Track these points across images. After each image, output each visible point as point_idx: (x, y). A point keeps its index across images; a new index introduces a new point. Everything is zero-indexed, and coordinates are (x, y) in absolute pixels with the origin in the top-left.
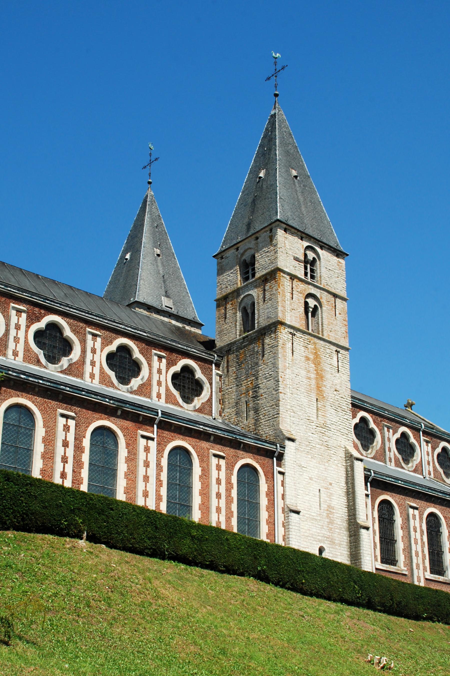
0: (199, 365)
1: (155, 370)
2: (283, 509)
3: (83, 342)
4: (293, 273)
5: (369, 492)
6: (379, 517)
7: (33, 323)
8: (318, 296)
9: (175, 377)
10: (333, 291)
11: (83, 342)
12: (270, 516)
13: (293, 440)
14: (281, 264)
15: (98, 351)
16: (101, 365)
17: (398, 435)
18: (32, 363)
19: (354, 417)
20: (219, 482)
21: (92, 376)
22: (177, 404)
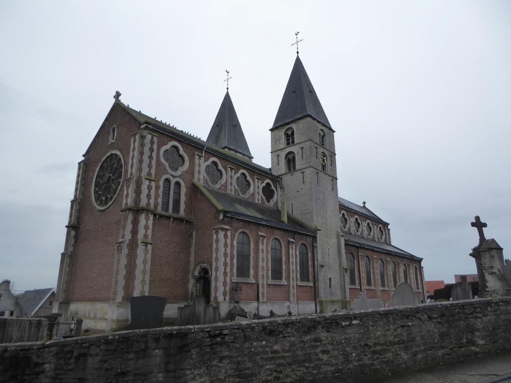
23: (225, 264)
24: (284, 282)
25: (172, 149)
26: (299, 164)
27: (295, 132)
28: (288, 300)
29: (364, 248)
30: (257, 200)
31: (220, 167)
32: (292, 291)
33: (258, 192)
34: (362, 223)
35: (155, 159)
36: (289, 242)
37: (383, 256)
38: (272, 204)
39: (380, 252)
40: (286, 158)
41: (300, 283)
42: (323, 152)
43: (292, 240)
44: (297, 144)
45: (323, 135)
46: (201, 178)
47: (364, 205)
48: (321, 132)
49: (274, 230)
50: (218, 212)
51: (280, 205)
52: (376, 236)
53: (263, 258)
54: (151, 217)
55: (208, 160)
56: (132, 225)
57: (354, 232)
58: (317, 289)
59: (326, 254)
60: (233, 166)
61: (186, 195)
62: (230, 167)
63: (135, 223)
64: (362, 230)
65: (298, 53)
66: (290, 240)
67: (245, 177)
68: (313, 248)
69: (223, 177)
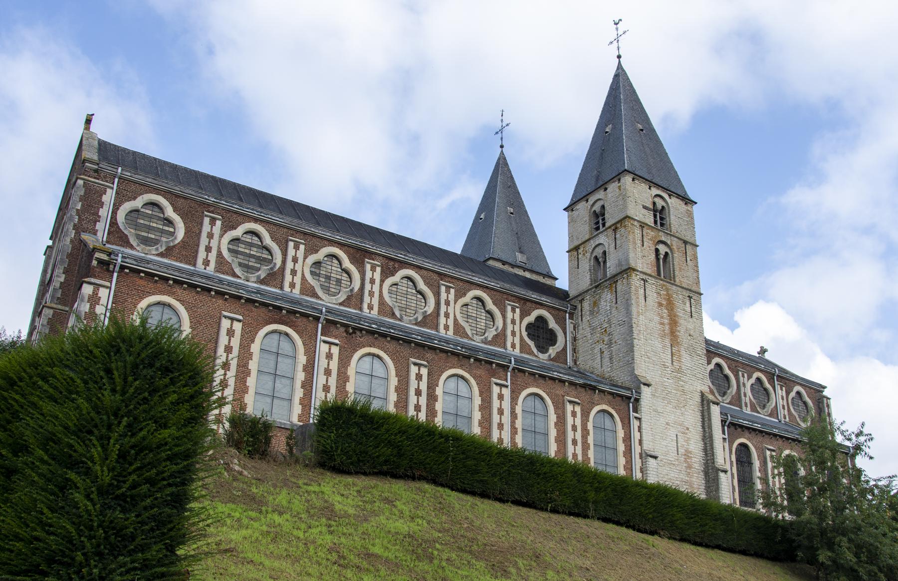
0: (553, 315)
1: (509, 321)
2: (641, 455)
3: (437, 295)
4: (643, 220)
5: (726, 437)
6: (737, 460)
7: (387, 277)
8: (669, 242)
9: (529, 327)
10: (683, 238)
11: (437, 295)
12: (627, 462)
13: (648, 385)
14: (631, 212)
15: (452, 303)
16: (455, 316)
17: (752, 381)
18: (386, 316)
19: (709, 363)
20: (574, 428)
21: (446, 327)
22: (532, 353)
25: (475, 301)
65: (619, 57)
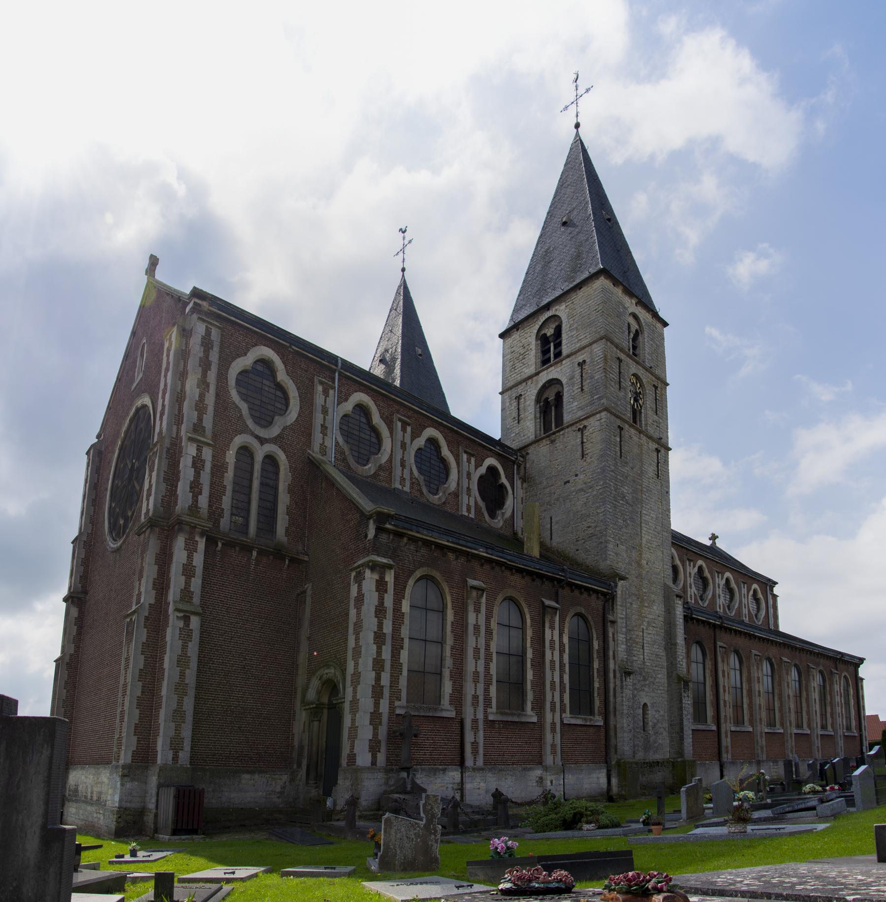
23: (378, 665)
24: (531, 717)
26: (571, 409)
27: (563, 325)
28: (541, 763)
29: (730, 630)
30: (465, 509)
31: (376, 419)
32: (549, 737)
33: (468, 489)
34: (713, 578)
35: (212, 389)
36: (545, 607)
37: (773, 651)
38: (501, 524)
39: (768, 640)
40: (538, 400)
41: (568, 718)
42: (635, 375)
43: (553, 604)
44: (568, 356)
45: (637, 331)
46: (328, 443)
47: (714, 543)
48: (631, 320)
49: (507, 573)
50: (365, 518)
51: (519, 524)
52: (745, 611)
53: (477, 650)
54: (201, 544)
55: (346, 400)
56: (156, 567)
57: (696, 600)
58: (612, 733)
59: (637, 643)
60: (408, 417)
61: (291, 490)
62: (400, 420)
63: (164, 560)
64: (714, 596)
66: (547, 602)
67: (438, 448)
68: (605, 623)
69: (383, 448)
